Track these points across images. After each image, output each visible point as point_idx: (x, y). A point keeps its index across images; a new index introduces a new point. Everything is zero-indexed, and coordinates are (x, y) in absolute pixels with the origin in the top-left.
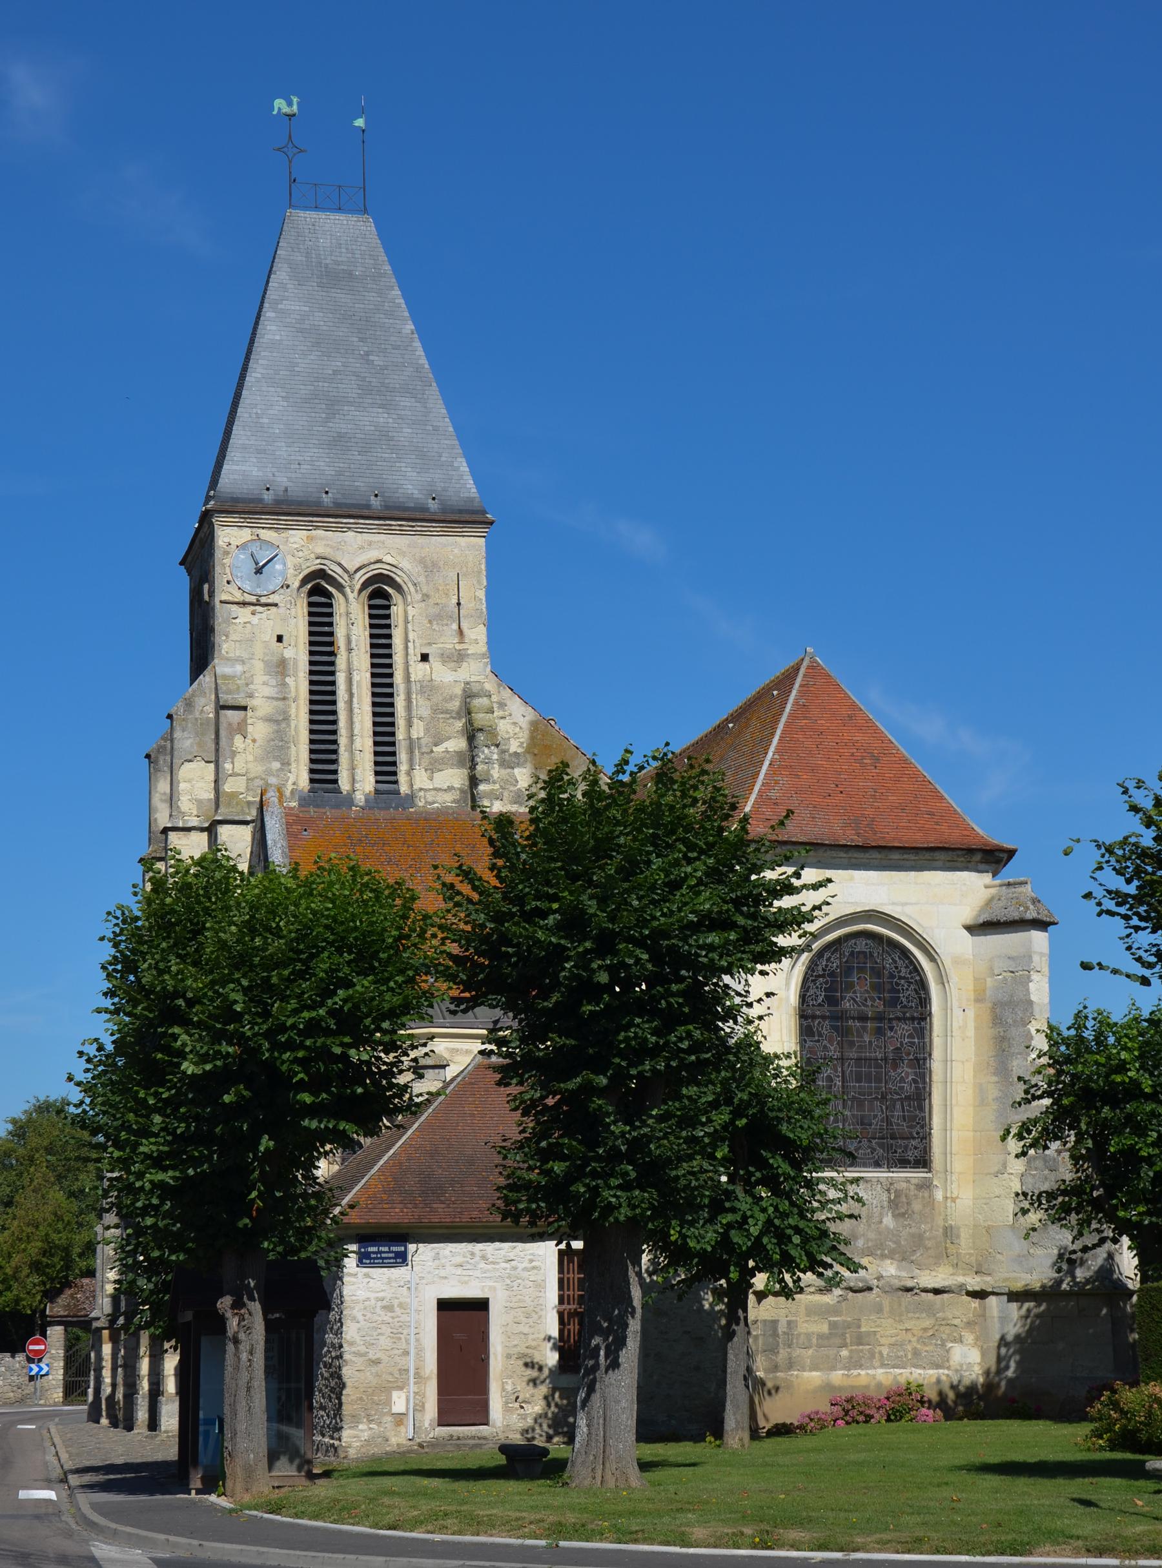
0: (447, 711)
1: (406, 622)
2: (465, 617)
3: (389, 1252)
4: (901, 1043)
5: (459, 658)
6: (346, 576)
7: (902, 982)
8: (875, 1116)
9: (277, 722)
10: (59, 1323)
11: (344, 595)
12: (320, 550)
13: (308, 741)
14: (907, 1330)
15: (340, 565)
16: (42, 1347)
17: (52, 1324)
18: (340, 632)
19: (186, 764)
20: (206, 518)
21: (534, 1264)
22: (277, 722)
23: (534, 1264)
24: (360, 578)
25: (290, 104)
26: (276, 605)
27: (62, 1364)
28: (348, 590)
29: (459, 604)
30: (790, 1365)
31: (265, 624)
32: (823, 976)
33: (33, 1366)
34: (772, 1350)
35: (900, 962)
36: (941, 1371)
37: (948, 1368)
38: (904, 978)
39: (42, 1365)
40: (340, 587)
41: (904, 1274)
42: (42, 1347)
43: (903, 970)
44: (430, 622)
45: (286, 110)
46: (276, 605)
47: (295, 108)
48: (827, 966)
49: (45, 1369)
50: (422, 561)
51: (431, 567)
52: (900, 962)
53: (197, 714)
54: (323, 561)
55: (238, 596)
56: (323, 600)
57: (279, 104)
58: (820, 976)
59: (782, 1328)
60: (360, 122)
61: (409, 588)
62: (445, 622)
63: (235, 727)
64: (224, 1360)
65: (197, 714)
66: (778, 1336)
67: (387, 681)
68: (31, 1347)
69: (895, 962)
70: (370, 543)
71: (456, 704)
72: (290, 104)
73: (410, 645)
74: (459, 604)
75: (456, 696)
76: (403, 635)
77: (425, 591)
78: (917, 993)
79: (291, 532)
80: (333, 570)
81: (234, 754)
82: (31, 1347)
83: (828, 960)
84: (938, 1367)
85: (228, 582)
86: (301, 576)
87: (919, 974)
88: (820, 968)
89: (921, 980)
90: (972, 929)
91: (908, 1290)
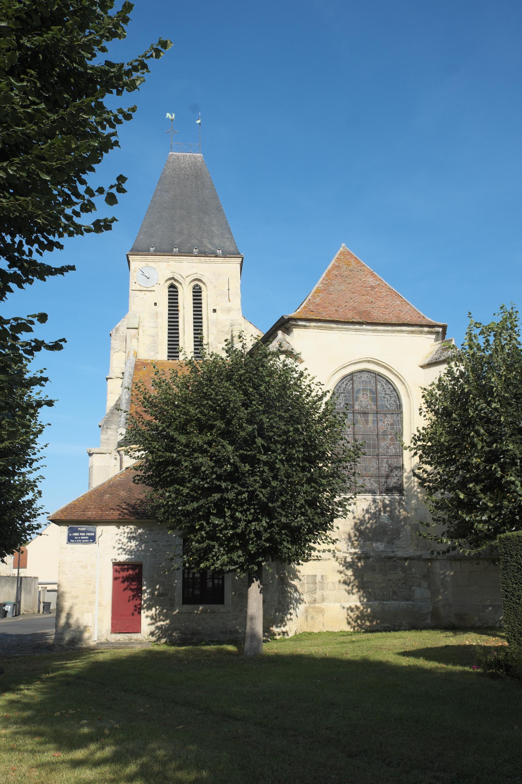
0: (223, 332)
1: (207, 297)
3: (86, 536)
4: (387, 428)
5: (229, 310)
6: (182, 279)
7: (387, 396)
8: (373, 466)
9: (153, 336)
13: (167, 345)
14: (389, 580)
15: (180, 275)
18: (180, 301)
19: (116, 353)
20: (127, 255)
21: (169, 543)
22: (153, 336)
23: (169, 543)
25: (172, 116)
28: (183, 285)
30: (323, 600)
31: (151, 298)
32: (343, 393)
34: (313, 591)
35: (385, 386)
36: (409, 602)
37: (413, 601)
38: (388, 394)
41: (388, 550)
43: (388, 390)
45: (170, 117)
47: (173, 117)
48: (345, 388)
52: (385, 386)
53: (121, 334)
56: (175, 290)
57: (168, 115)
58: (341, 393)
59: (319, 579)
60: (198, 122)
65: (121, 334)
66: (316, 584)
67: (200, 320)
69: (382, 386)
71: (227, 329)
72: (172, 116)
78: (395, 402)
80: (177, 277)
83: (346, 385)
84: (407, 600)
87: (396, 392)
88: (342, 389)
89: (397, 395)
90: (422, 367)
91: (390, 558)
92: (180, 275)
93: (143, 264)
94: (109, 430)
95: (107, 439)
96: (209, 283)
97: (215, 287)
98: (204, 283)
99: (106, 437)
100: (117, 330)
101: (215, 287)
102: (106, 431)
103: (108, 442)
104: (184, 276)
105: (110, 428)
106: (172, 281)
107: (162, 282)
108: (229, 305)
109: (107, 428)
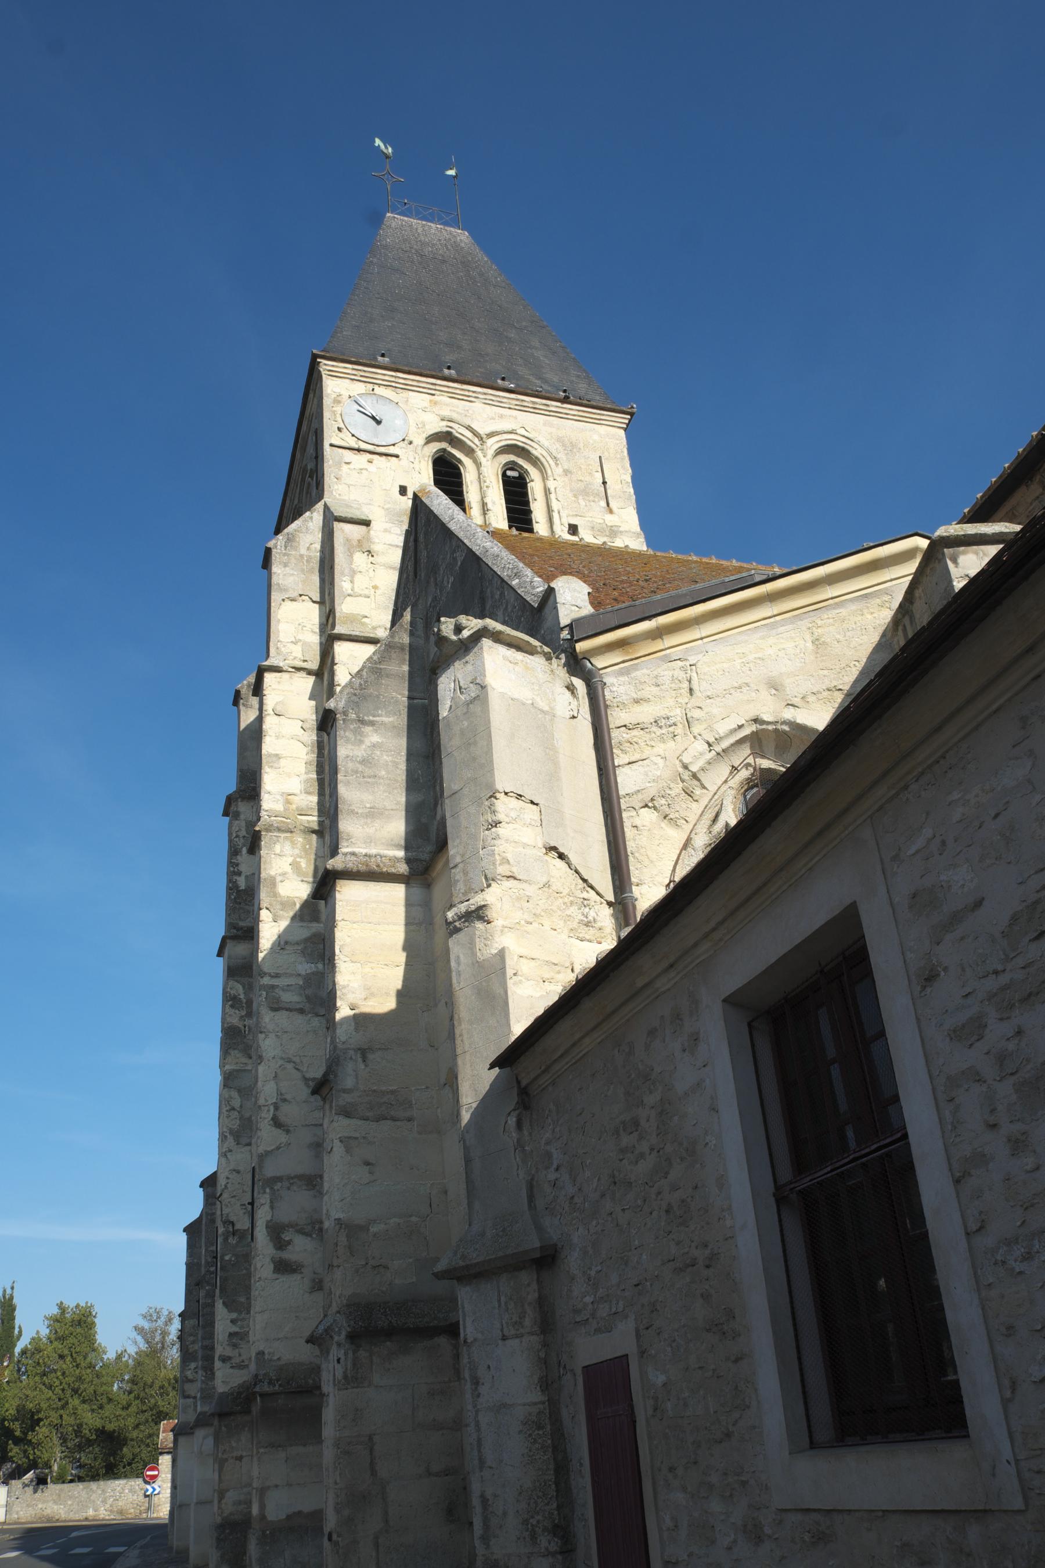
2: (613, 497)
6: (476, 441)
10: (168, 1453)
11: (478, 465)
12: (446, 412)
15: (469, 428)
16: (156, 1473)
17: (161, 1453)
19: (288, 603)
20: (315, 357)
24: (493, 445)
26: (397, 456)
27: (169, 1485)
28: (479, 454)
29: (604, 483)
33: (148, 1487)
39: (155, 1486)
40: (470, 452)
42: (156, 1473)
44: (575, 496)
46: (397, 456)
49: (158, 1490)
50: (559, 439)
51: (571, 447)
53: (303, 551)
54: (450, 424)
55: (353, 443)
60: (452, 172)
61: (548, 462)
62: (591, 498)
63: (355, 543)
64: (174, 1487)
68: (149, 1473)
70: (501, 416)
73: (555, 515)
74: (604, 483)
75: (500, 864)
76: (545, 509)
77: (566, 467)
79: (411, 393)
80: (459, 431)
81: (353, 573)
82: (149, 1473)
85: (339, 429)
86: (425, 435)
92: (469, 428)
93: (360, 388)
94: (368, 729)
95: (364, 762)
96: (551, 462)
97: (566, 472)
98: (535, 461)
99: (360, 752)
100: (290, 540)
101: (566, 472)
102: (357, 732)
103: (368, 771)
104: (483, 431)
105: (372, 723)
106: (444, 445)
107: (419, 440)
108: (610, 520)
109: (362, 722)
